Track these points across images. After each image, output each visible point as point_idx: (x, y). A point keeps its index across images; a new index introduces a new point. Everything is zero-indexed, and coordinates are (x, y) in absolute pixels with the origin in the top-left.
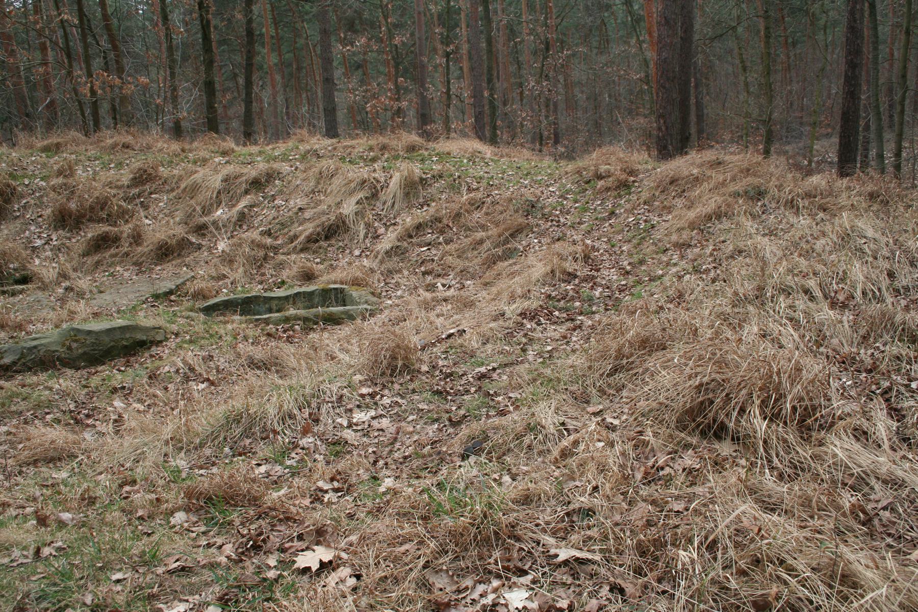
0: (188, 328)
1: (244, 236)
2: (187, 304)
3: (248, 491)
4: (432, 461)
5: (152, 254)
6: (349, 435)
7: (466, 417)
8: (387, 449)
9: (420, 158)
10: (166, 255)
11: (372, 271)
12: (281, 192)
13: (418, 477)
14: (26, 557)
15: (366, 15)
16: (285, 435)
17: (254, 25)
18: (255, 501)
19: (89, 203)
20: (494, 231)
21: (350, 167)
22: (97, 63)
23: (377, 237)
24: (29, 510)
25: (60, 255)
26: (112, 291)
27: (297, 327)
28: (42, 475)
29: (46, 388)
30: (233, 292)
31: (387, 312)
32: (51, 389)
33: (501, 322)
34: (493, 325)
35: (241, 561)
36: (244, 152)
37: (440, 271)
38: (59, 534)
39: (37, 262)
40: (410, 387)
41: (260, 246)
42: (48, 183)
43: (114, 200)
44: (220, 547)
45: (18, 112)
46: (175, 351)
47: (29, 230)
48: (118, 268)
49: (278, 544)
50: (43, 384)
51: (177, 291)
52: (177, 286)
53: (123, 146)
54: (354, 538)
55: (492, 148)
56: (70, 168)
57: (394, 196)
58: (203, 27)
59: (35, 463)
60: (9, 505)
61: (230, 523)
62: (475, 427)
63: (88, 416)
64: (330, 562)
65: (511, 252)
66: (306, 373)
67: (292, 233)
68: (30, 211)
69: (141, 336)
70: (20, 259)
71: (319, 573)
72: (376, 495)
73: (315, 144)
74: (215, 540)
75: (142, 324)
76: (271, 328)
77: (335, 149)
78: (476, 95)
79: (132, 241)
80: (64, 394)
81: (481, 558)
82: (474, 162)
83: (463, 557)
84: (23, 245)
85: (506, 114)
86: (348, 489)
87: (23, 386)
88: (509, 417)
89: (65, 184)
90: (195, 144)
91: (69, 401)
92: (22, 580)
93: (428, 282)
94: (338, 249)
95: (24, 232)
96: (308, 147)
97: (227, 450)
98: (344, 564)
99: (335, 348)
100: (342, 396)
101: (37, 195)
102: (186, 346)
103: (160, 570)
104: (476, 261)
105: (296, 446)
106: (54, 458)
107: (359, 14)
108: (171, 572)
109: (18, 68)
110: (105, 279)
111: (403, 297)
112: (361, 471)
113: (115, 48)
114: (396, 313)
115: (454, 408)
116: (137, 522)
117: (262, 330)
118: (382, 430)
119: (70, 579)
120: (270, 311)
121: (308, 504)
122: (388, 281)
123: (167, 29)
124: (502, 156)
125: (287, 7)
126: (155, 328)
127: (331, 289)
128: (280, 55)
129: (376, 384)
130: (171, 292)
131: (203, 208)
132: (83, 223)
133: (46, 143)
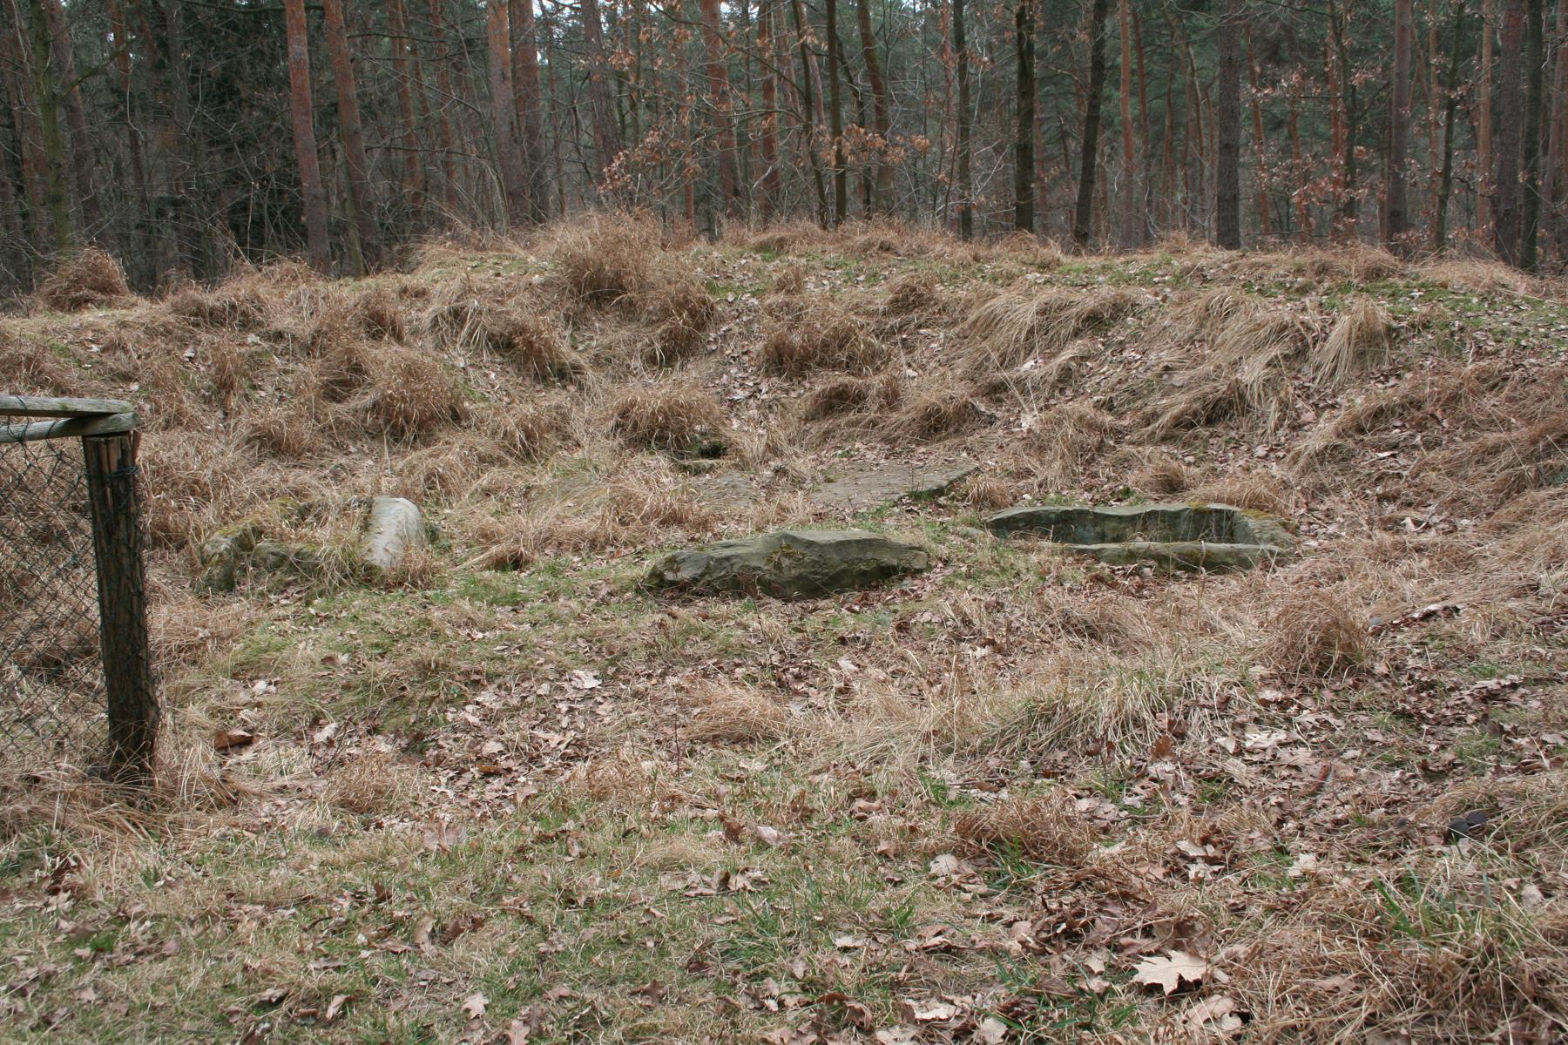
0: (966, 553)
1: (1068, 407)
2: (964, 514)
3: (1061, 838)
4: (1388, 836)
5: (914, 426)
6: (1236, 767)
7: (1455, 766)
8: (1303, 802)
9: (1390, 292)
10: (936, 430)
11: (1286, 485)
12: (1135, 337)
13: (1360, 861)
14: (708, 885)
15: (1302, 33)
16: (1125, 752)
17: (1106, 51)
18: (1071, 857)
19: (821, 337)
20: (1522, 432)
21: (1258, 300)
22: (847, 111)
23: (1296, 427)
24: (710, 813)
26: (847, 480)
27: (1147, 570)
28: (724, 761)
30: (1042, 500)
31: (1309, 560)
32: (745, 627)
33: (1530, 601)
34: (1513, 604)
35: (1044, 953)
36: (1076, 266)
37: (1412, 498)
38: (757, 859)
39: (736, 424)
40: (1353, 699)
41: (1093, 426)
42: (762, 301)
43: (861, 335)
44: (1009, 924)
45: (724, 186)
46: (942, 588)
47: (728, 373)
48: (858, 445)
49: (1108, 937)
50: (735, 618)
51: (950, 490)
52: (951, 482)
53: (881, 247)
54: (1241, 949)
55: (1527, 278)
56: (798, 279)
57: (1336, 357)
58: (1021, 54)
59: (715, 739)
60: (680, 801)
61: (1028, 887)
62: (1477, 786)
63: (798, 678)
64: (1198, 983)
65: (1554, 474)
66: (1166, 650)
67: (1148, 409)
69: (889, 559)
70: (711, 418)
71: (1175, 997)
72: (1282, 881)
73: (1200, 257)
74: (1001, 910)
75: (893, 539)
76: (1103, 568)
77: (1235, 267)
78: (1504, 179)
79: (884, 402)
80: (767, 639)
81: (1475, 1027)
82: (1492, 303)
83: (1440, 1019)
84: (717, 397)
85: (1555, 216)
86: (1231, 862)
87: (706, 618)
88: (1542, 778)
89: (787, 305)
90: (997, 249)
91: (771, 650)
92: (702, 920)
93: (1387, 514)
94: (1227, 442)
95: (721, 377)
96: (1188, 263)
97: (1025, 763)
98: (1222, 990)
99: (1215, 613)
100: (1228, 699)
101: (745, 319)
102: (960, 582)
103: (912, 944)
104: (1482, 484)
105: (1144, 775)
106: (744, 737)
107: (1289, 30)
108: (929, 951)
109: (729, 120)
110: (836, 460)
111: (1338, 537)
112: (1256, 835)
113: (877, 88)
114: (1325, 563)
115: (1433, 747)
116: (877, 861)
117: (1088, 569)
118: (1296, 768)
119: (773, 931)
120: (1102, 538)
121: (1160, 877)
122: (1312, 505)
123: (963, 57)
124: (1548, 295)
125: (1162, 20)
126: (913, 548)
127: (1211, 511)
128: (1143, 103)
129: (1290, 686)
130: (940, 491)
131: (1003, 357)
132: (809, 368)
133: (764, 237)
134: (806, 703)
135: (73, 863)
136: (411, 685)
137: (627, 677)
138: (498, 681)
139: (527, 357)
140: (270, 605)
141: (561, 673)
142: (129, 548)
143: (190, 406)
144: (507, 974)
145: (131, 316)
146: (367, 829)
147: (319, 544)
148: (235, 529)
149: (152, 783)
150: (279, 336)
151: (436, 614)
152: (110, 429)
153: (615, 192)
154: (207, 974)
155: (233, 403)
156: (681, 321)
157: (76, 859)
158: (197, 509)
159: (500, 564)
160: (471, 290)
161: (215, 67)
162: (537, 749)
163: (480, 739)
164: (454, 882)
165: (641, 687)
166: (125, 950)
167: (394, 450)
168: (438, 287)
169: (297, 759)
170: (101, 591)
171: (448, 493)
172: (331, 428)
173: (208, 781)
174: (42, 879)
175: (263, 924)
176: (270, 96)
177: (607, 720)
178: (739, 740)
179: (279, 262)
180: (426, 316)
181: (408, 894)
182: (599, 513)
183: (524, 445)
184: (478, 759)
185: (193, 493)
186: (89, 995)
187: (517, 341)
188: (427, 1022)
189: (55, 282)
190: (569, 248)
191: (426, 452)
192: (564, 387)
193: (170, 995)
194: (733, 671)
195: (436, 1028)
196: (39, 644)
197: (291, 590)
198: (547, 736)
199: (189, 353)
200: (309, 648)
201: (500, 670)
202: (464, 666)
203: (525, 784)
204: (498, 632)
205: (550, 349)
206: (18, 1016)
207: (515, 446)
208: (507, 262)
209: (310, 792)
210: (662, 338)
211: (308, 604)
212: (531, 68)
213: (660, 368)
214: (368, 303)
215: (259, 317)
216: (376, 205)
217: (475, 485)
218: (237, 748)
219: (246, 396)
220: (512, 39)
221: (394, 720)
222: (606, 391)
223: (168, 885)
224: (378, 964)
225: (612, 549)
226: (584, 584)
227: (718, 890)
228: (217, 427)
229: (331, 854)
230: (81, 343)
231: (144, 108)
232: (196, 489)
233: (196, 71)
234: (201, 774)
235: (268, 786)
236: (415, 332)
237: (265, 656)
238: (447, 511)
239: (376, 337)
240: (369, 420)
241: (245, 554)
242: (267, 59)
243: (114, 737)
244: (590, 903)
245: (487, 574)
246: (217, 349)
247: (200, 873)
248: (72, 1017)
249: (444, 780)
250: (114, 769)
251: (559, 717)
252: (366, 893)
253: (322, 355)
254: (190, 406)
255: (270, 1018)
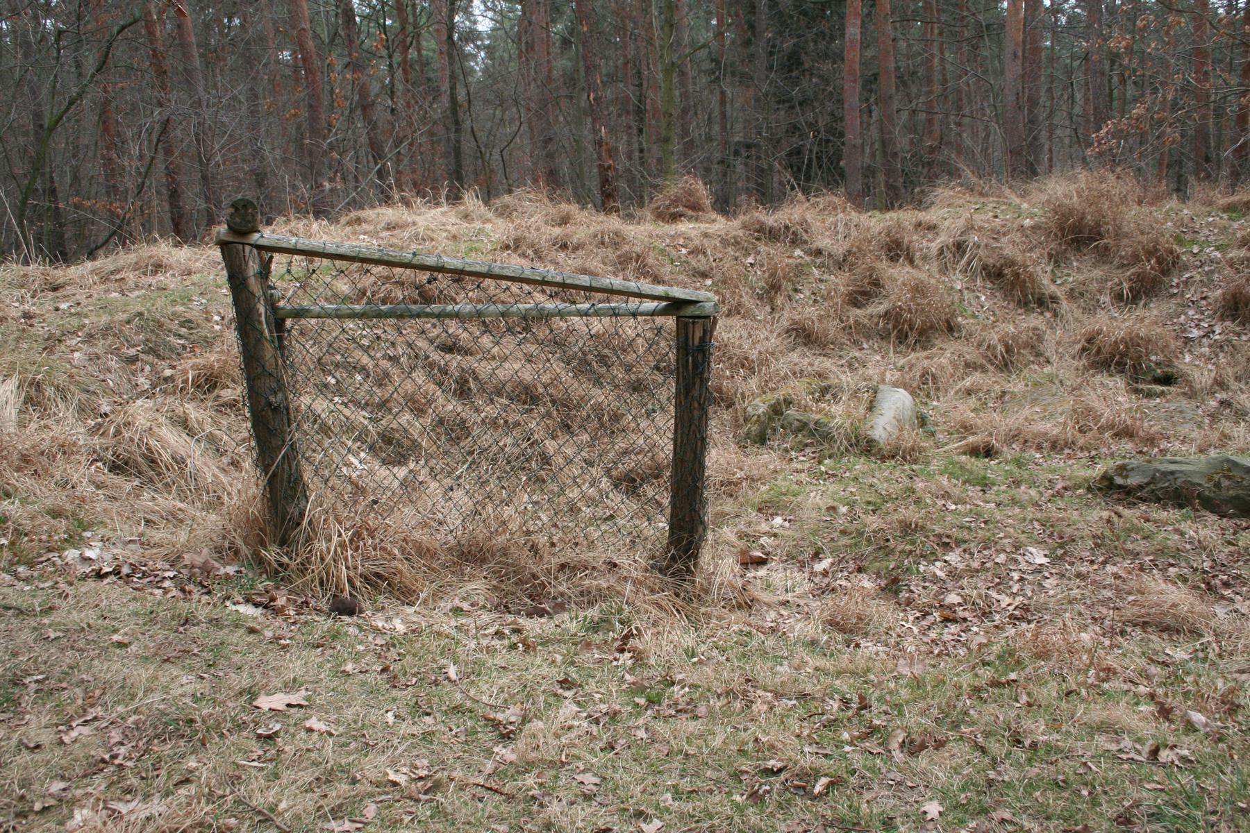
14: (1139, 753)
25: (1221, 355)
29: (1177, 531)
32: (1182, 534)
39: (1188, 358)
47: (1186, 314)
59: (1144, 625)
63: (1226, 585)
68: (1193, 289)
70: (1166, 350)
80: (1201, 547)
84: (1173, 334)
87: (1147, 520)
101: (1207, 269)
106: (1172, 628)
109: (1208, 97)
119: (1197, 806)
134: (1231, 608)
135: (635, 632)
136: (894, 538)
137: (1073, 559)
138: (965, 546)
139: (1013, 285)
140: (792, 460)
141: (1017, 548)
142: (699, 404)
143: (748, 301)
144: (959, 790)
145: (711, 229)
146: (848, 647)
147: (833, 417)
148: (771, 397)
149: (694, 582)
150: (819, 252)
151: (919, 485)
152: (697, 313)
153: (1101, 154)
154: (727, 738)
155: (779, 300)
156: (1149, 266)
157: (637, 629)
158: (745, 379)
159: (974, 452)
160: (973, 228)
161: (788, 44)
162: (990, 607)
163: (944, 590)
164: (922, 705)
165: (1083, 570)
166: (669, 706)
167: (898, 350)
168: (947, 223)
169: (799, 580)
170: (676, 432)
171: (938, 389)
172: (851, 328)
173: (732, 587)
174: (614, 640)
175: (771, 708)
176: (826, 67)
177: (1051, 593)
178: (1166, 629)
179: (824, 195)
180: (935, 246)
181: (884, 708)
182: (1061, 420)
183: (1003, 357)
184: (941, 606)
185: (743, 366)
186: (641, 734)
187: (1006, 272)
188: (892, 814)
189: (661, 200)
190: (1057, 199)
191: (924, 354)
192: (1042, 313)
193: (700, 748)
194: (1166, 570)
195: (898, 821)
196: (629, 464)
197: (808, 450)
198: (999, 597)
199: (750, 260)
200: (818, 497)
201: (967, 537)
202: (938, 530)
203: (976, 634)
204: (968, 507)
205: (1033, 281)
206: (593, 738)
207: (996, 357)
208: (1003, 207)
209: (806, 609)
210: (1131, 280)
211: (820, 462)
212: (1036, 50)
213: (1126, 305)
214: (890, 232)
215: (805, 237)
216: (900, 154)
217: (960, 385)
218: (755, 566)
219: (789, 296)
220: (1025, 25)
221: (877, 564)
222: (1076, 320)
223: (701, 662)
224: (858, 760)
225: (1070, 451)
226: (1044, 477)
227: (1148, 759)
228: (766, 318)
229: (821, 662)
230: (675, 247)
231: (733, 74)
232: (745, 364)
233: (774, 46)
234: (729, 581)
235: (775, 599)
236: (925, 258)
237: (784, 498)
238: (935, 403)
239: (894, 259)
240: (881, 324)
241: (777, 418)
242: (827, 39)
243: (671, 543)
244: (1034, 746)
245: (963, 458)
246: (772, 259)
247: (724, 658)
248: (629, 747)
249: (911, 618)
250: (668, 567)
251: (1011, 583)
252: (851, 699)
253: (850, 270)
254: (748, 301)
255: (771, 783)
